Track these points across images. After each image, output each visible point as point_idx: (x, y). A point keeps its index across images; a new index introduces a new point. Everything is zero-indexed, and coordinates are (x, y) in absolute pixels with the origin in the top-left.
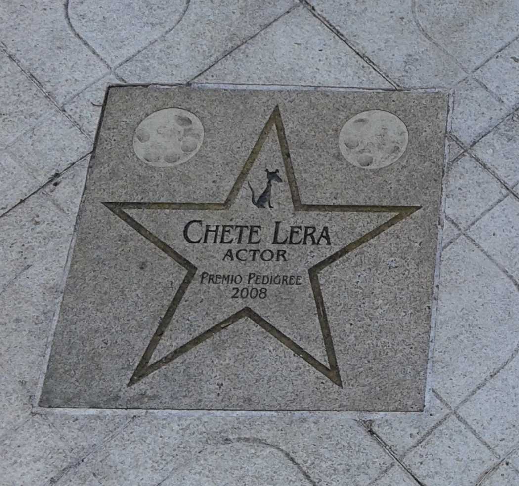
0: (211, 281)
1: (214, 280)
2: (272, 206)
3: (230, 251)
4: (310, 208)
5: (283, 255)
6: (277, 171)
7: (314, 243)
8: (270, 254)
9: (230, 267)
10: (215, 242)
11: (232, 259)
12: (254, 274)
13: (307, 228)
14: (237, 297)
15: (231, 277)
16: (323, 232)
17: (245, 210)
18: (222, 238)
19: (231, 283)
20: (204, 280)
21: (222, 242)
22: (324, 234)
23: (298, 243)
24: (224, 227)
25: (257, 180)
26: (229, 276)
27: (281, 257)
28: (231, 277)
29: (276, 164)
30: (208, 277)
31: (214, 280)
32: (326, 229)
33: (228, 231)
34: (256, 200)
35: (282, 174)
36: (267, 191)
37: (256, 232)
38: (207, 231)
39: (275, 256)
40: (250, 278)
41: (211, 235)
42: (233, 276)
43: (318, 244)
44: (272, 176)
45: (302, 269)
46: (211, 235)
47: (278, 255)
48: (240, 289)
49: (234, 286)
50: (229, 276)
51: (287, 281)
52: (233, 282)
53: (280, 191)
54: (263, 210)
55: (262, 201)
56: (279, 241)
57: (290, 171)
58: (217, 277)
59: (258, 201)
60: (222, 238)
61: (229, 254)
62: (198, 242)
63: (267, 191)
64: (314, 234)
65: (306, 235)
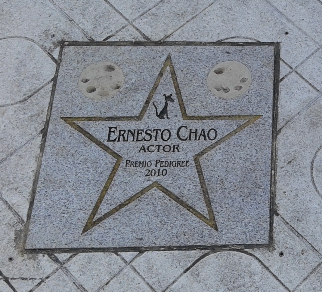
0: (132, 166)
1: (181, 164)
2: (169, 117)
3: (143, 146)
4: (192, 118)
5: (177, 148)
6: (171, 95)
7: (124, 140)
8: (169, 148)
9: (142, 157)
10: (196, 139)
11: (145, 152)
12: (159, 160)
13: (120, 131)
14: (149, 176)
15: (144, 163)
16: (201, 133)
17: (151, 121)
18: (137, 138)
19: (145, 166)
20: (127, 165)
21: (137, 140)
22: (202, 134)
23: (114, 140)
24: (138, 130)
25: (159, 100)
26: (143, 162)
27: (176, 149)
28: (144, 163)
29: (172, 91)
30: (130, 163)
31: (181, 164)
32: (203, 130)
33: (114, 132)
34: (159, 112)
35: (174, 97)
36: (166, 107)
37: (141, 133)
38: (191, 132)
39: (172, 149)
40: (157, 163)
41: (193, 135)
42: (146, 162)
43: (127, 141)
44: (168, 98)
45: (190, 157)
46: (193, 135)
47: (174, 148)
48: (151, 170)
49: (147, 168)
50: (143, 162)
51: (179, 163)
52: (171, 165)
53: (174, 107)
54: (163, 120)
55: (162, 114)
56: (139, 139)
57: (179, 94)
58: (182, 163)
59: (160, 114)
60: (137, 138)
61: (143, 148)
62: (186, 140)
63: (166, 107)
64: (124, 135)
65: (120, 135)
